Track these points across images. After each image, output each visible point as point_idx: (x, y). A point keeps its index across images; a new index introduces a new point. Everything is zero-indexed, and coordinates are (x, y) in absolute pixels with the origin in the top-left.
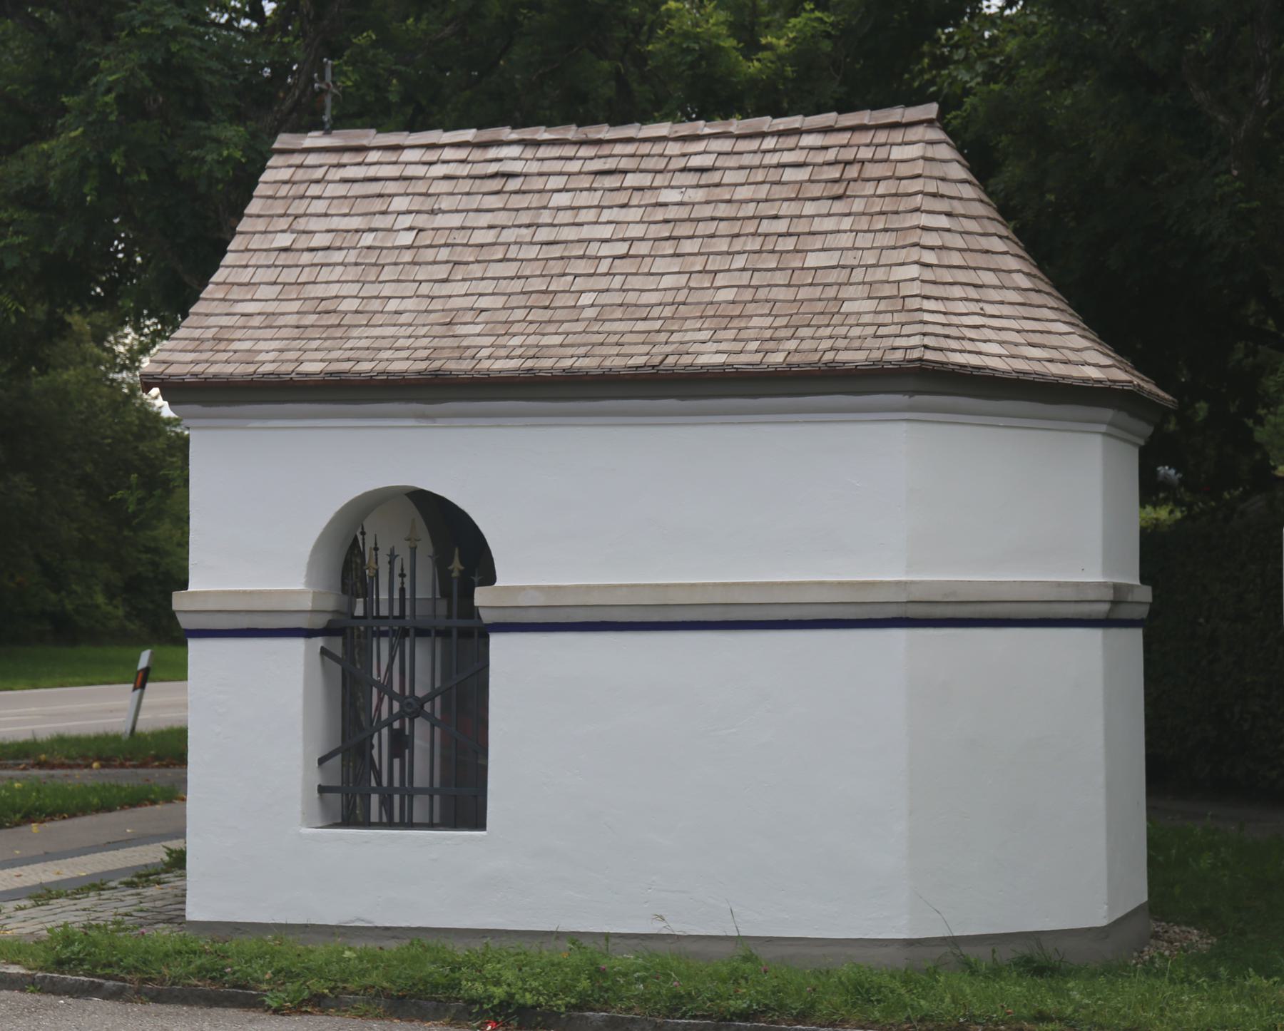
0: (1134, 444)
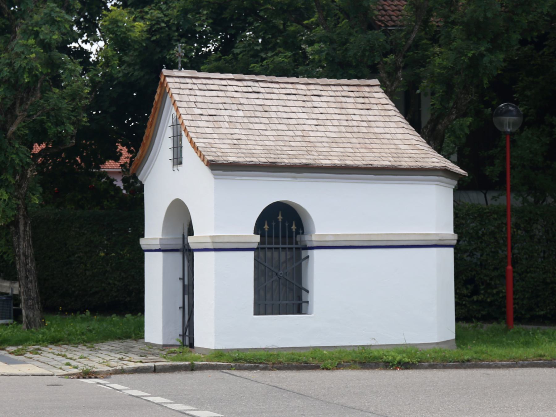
0: (451, 188)
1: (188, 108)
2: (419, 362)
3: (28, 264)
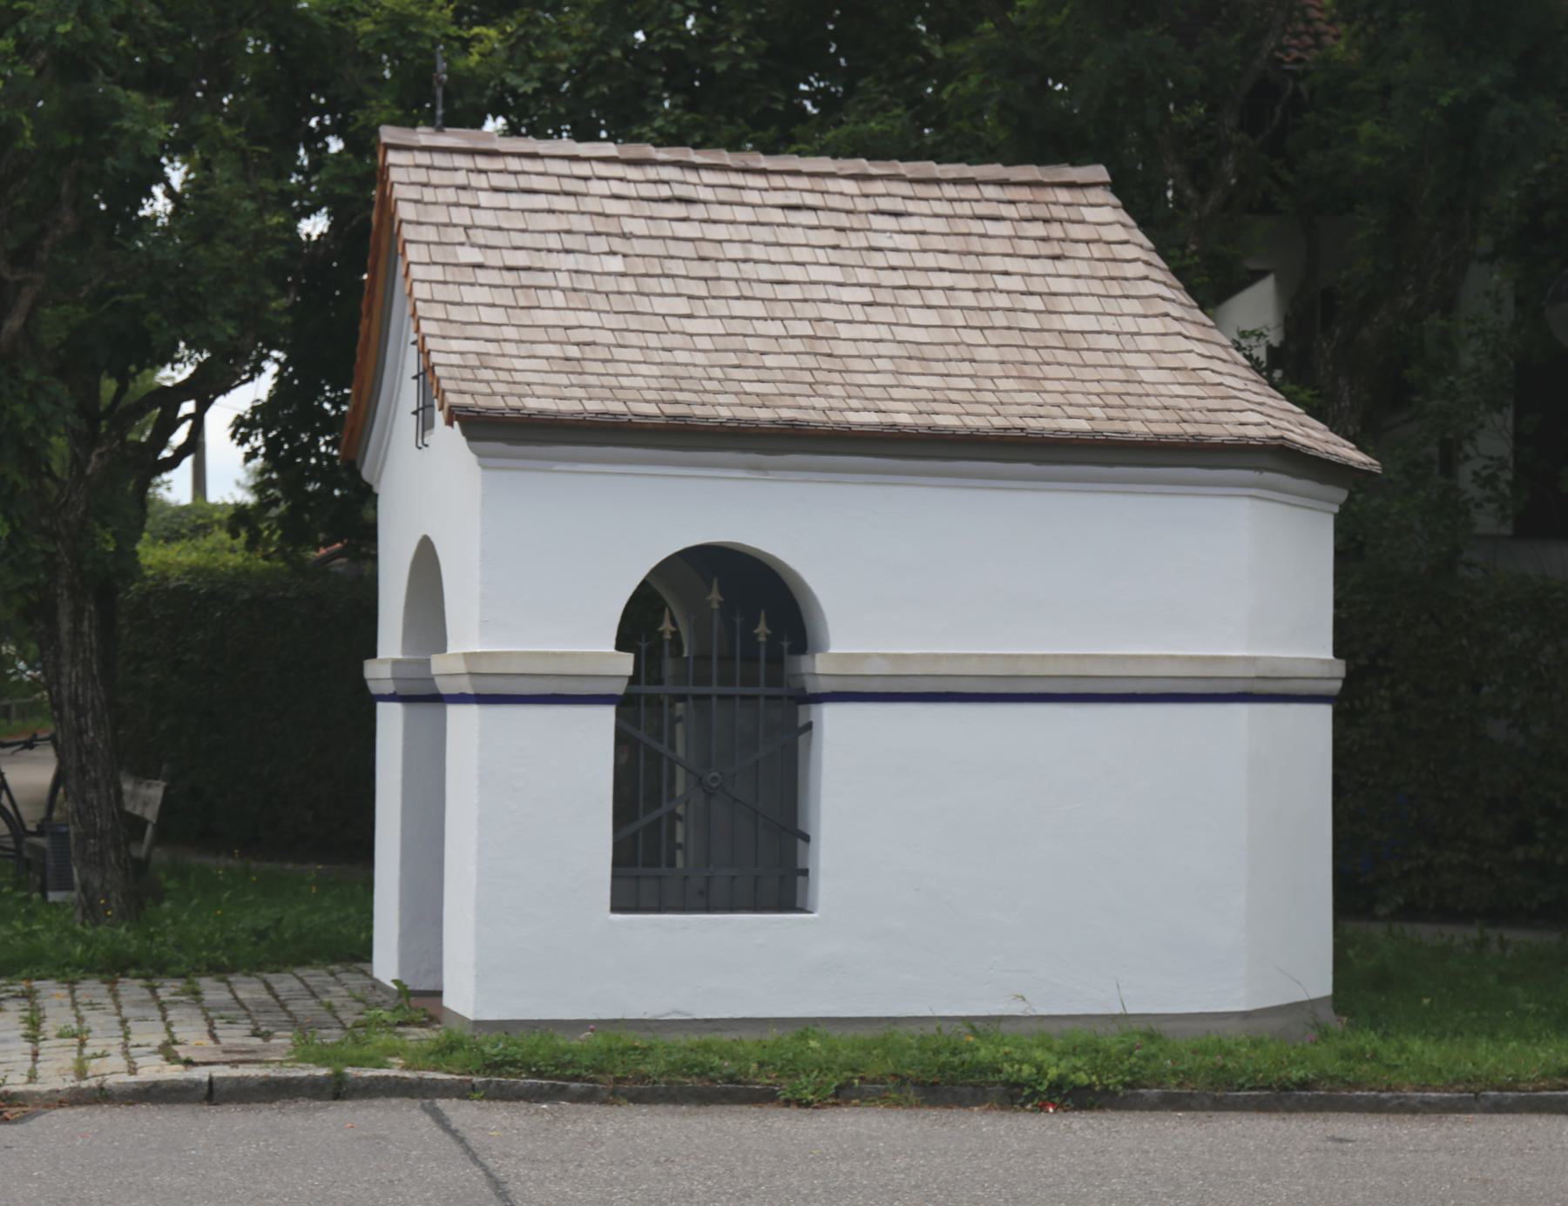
0: (1328, 512)
1: (440, 243)
2: (1126, 1085)
3: (86, 732)
